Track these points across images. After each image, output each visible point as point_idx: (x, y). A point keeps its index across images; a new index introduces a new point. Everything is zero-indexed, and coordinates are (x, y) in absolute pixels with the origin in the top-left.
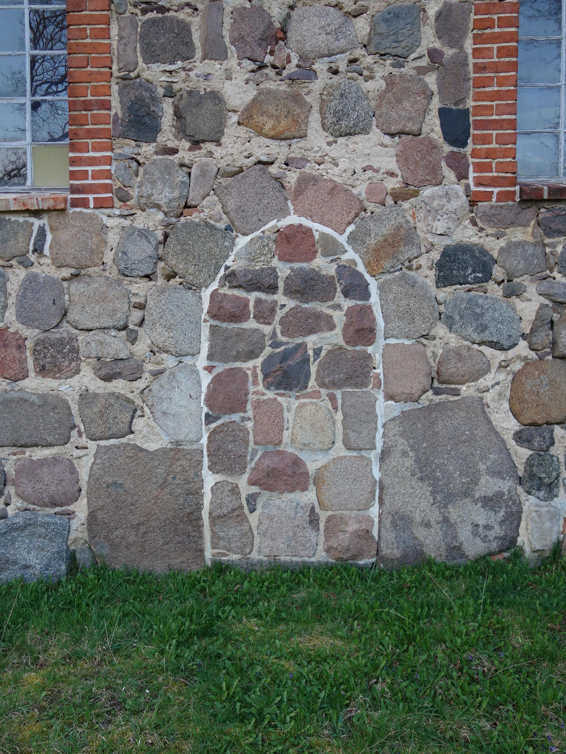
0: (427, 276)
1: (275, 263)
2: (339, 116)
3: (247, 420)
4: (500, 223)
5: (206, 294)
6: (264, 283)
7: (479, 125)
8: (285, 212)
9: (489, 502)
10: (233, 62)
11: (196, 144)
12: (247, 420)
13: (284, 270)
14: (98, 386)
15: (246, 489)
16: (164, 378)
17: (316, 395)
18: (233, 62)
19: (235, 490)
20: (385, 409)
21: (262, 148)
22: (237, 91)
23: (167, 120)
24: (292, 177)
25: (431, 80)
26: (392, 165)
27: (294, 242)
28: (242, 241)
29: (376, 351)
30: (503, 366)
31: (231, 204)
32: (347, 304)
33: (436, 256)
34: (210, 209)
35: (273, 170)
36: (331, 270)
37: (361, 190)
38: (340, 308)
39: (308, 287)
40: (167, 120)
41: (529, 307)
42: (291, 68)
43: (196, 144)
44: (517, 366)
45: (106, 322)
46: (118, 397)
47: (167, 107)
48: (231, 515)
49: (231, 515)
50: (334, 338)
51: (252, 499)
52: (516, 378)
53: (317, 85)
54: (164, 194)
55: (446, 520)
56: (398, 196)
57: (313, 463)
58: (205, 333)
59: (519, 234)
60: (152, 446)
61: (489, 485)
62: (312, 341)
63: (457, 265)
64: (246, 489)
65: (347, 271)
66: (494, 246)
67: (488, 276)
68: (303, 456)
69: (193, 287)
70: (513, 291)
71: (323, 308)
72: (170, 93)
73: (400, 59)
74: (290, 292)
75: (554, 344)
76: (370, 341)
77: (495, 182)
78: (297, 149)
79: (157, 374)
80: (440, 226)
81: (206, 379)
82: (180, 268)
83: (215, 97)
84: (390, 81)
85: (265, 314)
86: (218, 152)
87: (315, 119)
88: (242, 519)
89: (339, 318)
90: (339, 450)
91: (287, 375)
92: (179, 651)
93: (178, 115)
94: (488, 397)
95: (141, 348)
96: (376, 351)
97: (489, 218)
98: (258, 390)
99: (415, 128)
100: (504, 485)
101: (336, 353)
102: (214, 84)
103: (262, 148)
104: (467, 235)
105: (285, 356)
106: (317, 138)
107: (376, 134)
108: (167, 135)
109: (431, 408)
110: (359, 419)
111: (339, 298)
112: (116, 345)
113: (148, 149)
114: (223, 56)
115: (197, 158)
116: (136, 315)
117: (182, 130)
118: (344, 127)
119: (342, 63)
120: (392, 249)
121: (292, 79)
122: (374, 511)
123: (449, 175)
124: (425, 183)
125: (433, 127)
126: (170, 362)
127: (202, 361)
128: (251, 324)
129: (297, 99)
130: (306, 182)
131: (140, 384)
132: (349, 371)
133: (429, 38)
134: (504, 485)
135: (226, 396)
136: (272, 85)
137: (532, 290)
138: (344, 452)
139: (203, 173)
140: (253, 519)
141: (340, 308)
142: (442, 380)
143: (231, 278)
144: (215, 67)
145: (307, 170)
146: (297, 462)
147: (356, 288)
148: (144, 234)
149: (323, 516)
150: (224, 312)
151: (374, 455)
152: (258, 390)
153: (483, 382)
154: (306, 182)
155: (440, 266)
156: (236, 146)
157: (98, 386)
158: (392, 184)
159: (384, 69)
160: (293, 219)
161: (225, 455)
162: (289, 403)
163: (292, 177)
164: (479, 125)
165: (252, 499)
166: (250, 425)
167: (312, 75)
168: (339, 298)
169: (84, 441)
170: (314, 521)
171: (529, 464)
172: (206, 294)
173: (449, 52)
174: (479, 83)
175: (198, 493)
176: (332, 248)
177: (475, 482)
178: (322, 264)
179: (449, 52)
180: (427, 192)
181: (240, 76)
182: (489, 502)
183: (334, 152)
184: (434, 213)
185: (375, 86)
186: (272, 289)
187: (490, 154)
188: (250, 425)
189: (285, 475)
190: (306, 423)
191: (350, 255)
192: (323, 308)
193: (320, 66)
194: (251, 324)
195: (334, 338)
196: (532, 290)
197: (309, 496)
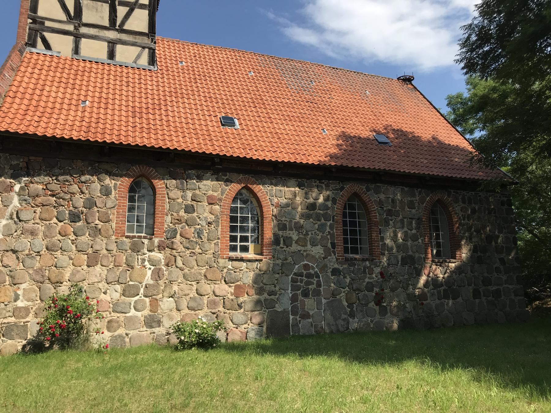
0: (329, 274)
1: (303, 271)
2: (313, 242)
3: (298, 304)
4: (341, 264)
5: (290, 277)
6: (301, 275)
7: (337, 245)
8: (304, 261)
9: (344, 320)
10: (294, 231)
11: (287, 247)
12: (298, 304)
13: (305, 272)
14: (268, 297)
15: (299, 319)
16: (282, 295)
17: (311, 298)
18: (294, 231)
19: (296, 319)
20: (324, 301)
21: (299, 248)
22: (295, 237)
23: (282, 242)
24: (305, 254)
25: (329, 237)
26: (323, 252)
27: (306, 267)
28: (297, 266)
29: (321, 289)
30: (344, 292)
31: (294, 259)
32: (316, 279)
33: (331, 270)
34: (290, 259)
35: (302, 252)
36: (313, 273)
37: (317, 257)
38: (315, 280)
39: (309, 276)
40: (282, 242)
41: (348, 280)
42: (304, 233)
43: (287, 247)
44: (346, 292)
45: (271, 283)
46: (272, 299)
47: (282, 239)
48: (296, 325)
49: (296, 325)
50: (314, 286)
51: (300, 321)
52: (346, 294)
53: (309, 236)
54: (282, 257)
55: (336, 324)
56: (324, 258)
57: (311, 313)
58: (290, 285)
59: (345, 266)
60: (279, 310)
61: (344, 316)
62: (310, 287)
63: (335, 272)
64: (299, 319)
65: (316, 272)
66: (341, 268)
67: (340, 274)
68: (309, 311)
69: (287, 276)
70: (345, 277)
71: (312, 280)
72: (282, 236)
73: (323, 233)
74: (305, 277)
75: (352, 288)
76: (321, 287)
77: (340, 256)
78: (306, 248)
79: (280, 294)
80: (332, 264)
81: (290, 295)
82: (285, 272)
83: (291, 238)
84: (321, 236)
85: (301, 281)
86: (291, 248)
87: (309, 242)
88: (298, 326)
89: (315, 282)
90: (316, 310)
91: (306, 294)
92: (187, 401)
93: (284, 241)
94: (342, 298)
95: (277, 289)
96: (321, 289)
97: (340, 263)
98: (300, 297)
99: (244, 191)
100: (345, 316)
101: (315, 289)
102: (291, 235)
103: (299, 248)
104: (336, 266)
105: (305, 290)
106: (309, 247)
107: (319, 246)
108: (281, 245)
109: (332, 301)
110: (319, 303)
111: (315, 278)
112: (273, 288)
113: (278, 247)
114: (292, 230)
115: (288, 249)
116: (276, 281)
117: (284, 243)
118: (314, 244)
119: (313, 232)
120: (323, 268)
121: (304, 235)
122: (323, 322)
123: (333, 254)
124: (329, 256)
125: (329, 245)
126: (283, 292)
127: (289, 291)
128: (299, 283)
129: (306, 239)
130: (307, 255)
131: (277, 297)
132: (317, 293)
133: (328, 229)
134: (345, 316)
135: (294, 299)
136: (301, 236)
137: (348, 277)
138: (317, 310)
139: (289, 252)
140: (300, 325)
141: (315, 280)
142: (334, 295)
143: (295, 274)
144: (291, 232)
145: (307, 252)
146: (308, 313)
147: (318, 277)
148: (278, 264)
149: (314, 324)
150: (293, 281)
151: (322, 311)
152: (300, 297)
153: (341, 295)
154: (307, 255)
155: (332, 272)
156: (295, 247)
157: (268, 297)
158: (323, 256)
159: (321, 234)
160: (306, 262)
161: (294, 313)
162: (306, 300)
163: (305, 254)
164: (337, 245)
165: (300, 321)
166: (299, 305)
167: (308, 234)
168: (315, 278)
169: (265, 309)
170: (312, 325)
171: (350, 312)
172: (290, 277)
173: (332, 232)
174: (337, 238)
175: (289, 320)
176: (313, 268)
177: (341, 316)
178: (312, 271)
179: (332, 232)
180: (329, 257)
181: (295, 234)
182: (344, 320)
183: (313, 249)
184: (331, 262)
185: (319, 237)
186: (303, 276)
187: (339, 251)
188: (299, 305)
189: (305, 316)
190: (310, 304)
191: (316, 270)
192: (312, 280)
193: (310, 233)
194: (299, 283)
195: (314, 286)
196: (348, 277)
197: (311, 320)
